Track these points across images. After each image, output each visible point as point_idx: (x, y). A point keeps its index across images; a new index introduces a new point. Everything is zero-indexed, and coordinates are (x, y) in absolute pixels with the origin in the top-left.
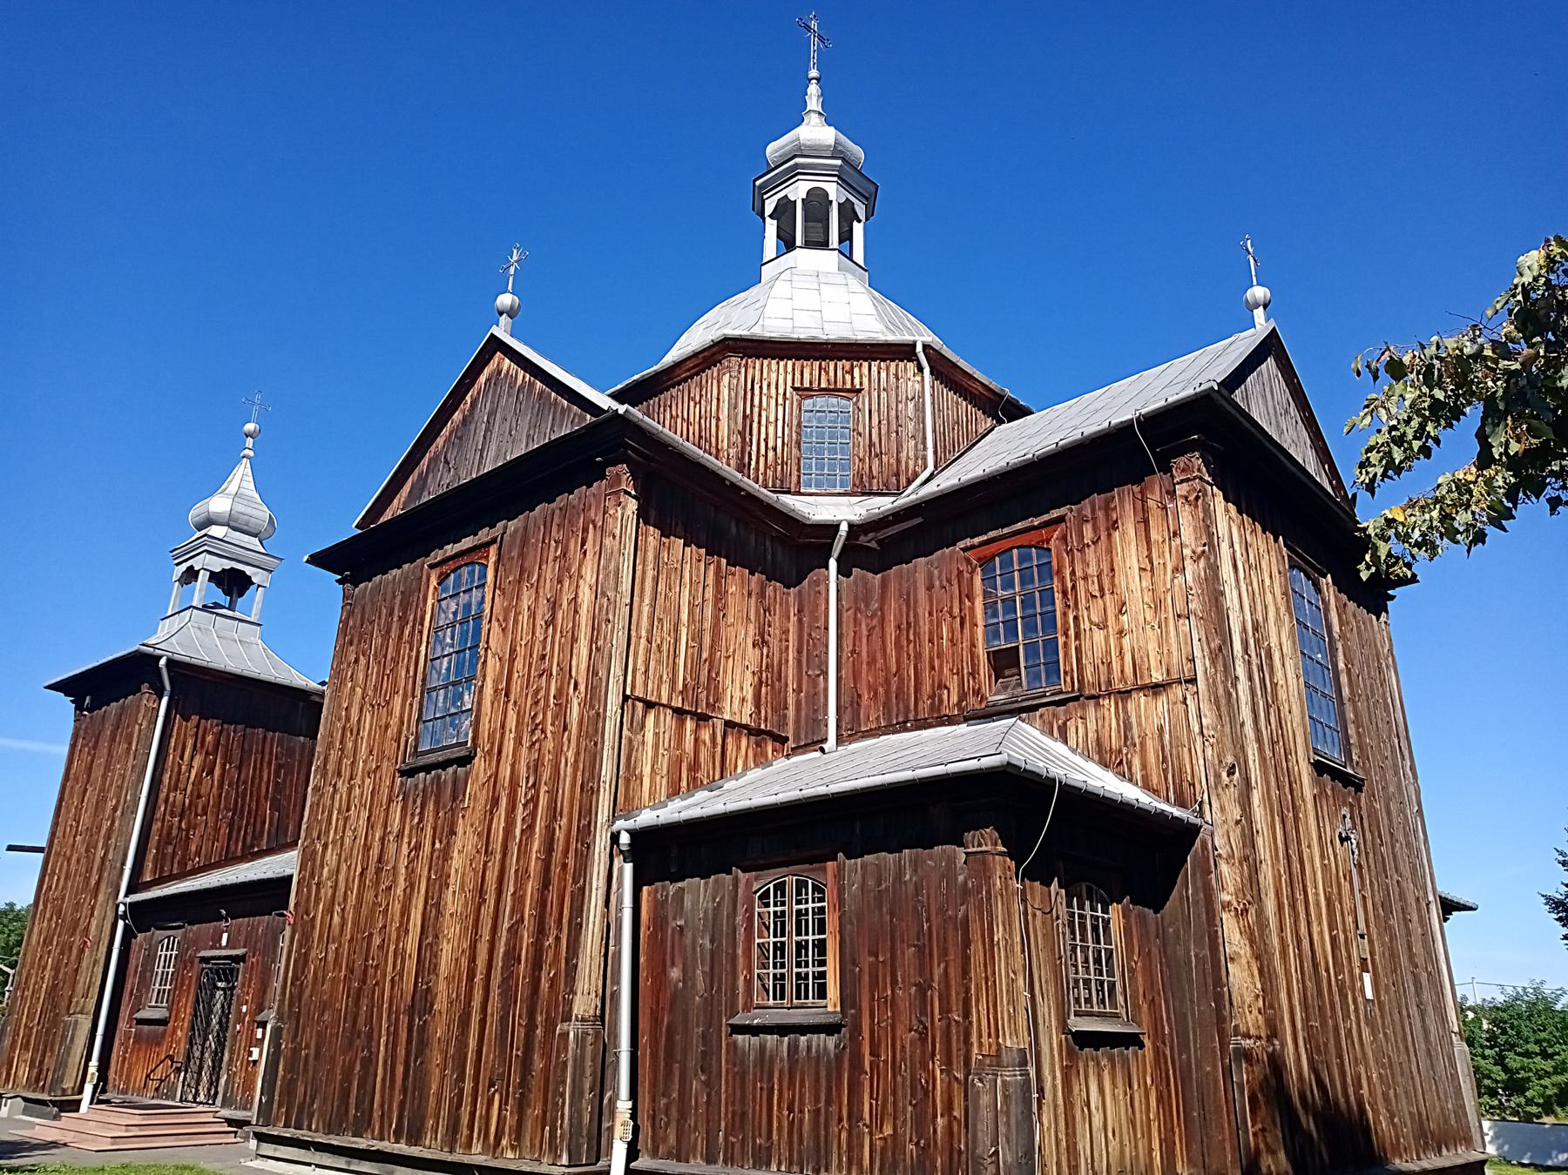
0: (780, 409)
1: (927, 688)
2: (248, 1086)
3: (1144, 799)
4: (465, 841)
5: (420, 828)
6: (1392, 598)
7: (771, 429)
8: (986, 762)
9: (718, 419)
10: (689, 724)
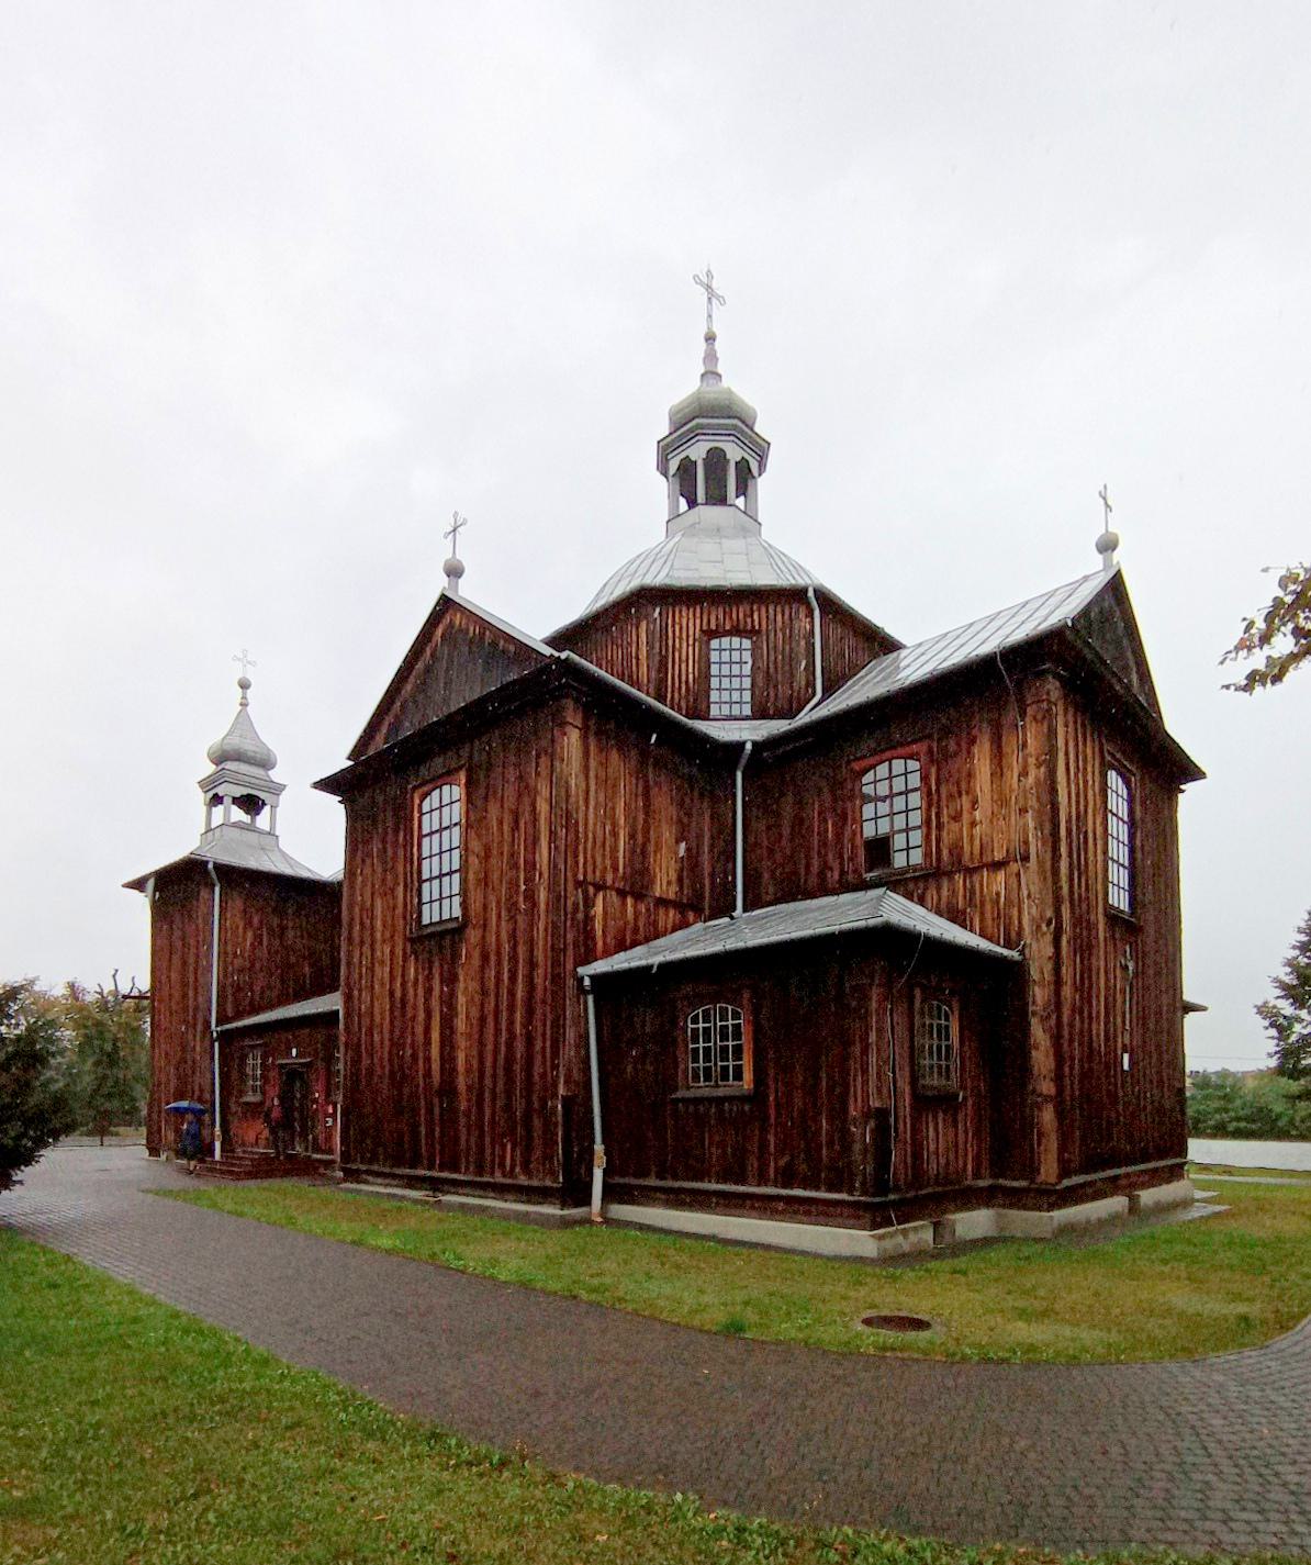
0: (691, 649)
1: (815, 868)
2: (329, 1138)
3: (984, 945)
4: (466, 988)
5: (429, 978)
6: (1183, 791)
7: (683, 666)
8: (872, 922)
9: (638, 659)
10: (629, 901)
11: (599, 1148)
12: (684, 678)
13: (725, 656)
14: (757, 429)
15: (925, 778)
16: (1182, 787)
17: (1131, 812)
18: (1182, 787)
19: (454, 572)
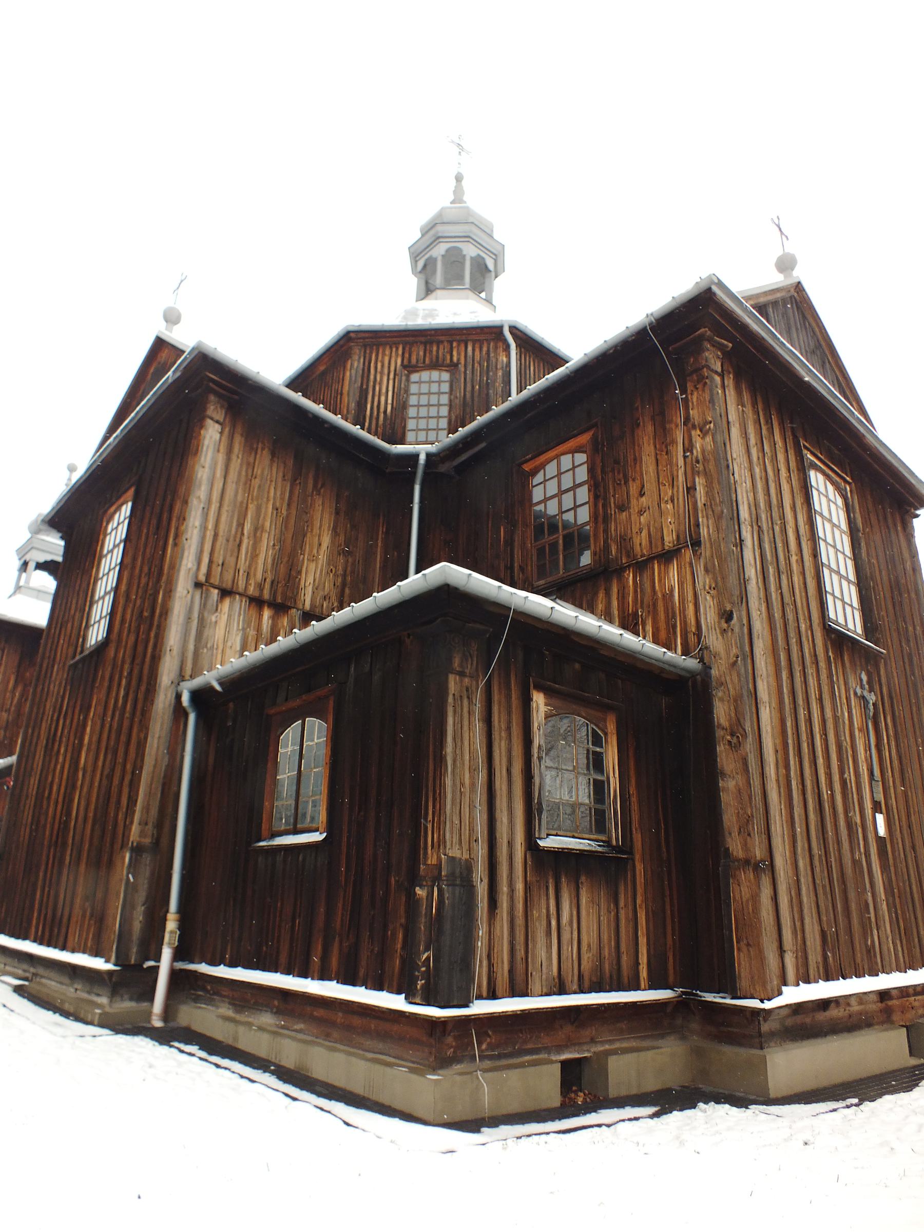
6: (917, 516)
11: (171, 925)
12: (382, 409)
13: (425, 388)
14: (496, 236)
15: (591, 471)
16: (918, 512)
17: (851, 522)
18: (918, 512)
19: (172, 318)
